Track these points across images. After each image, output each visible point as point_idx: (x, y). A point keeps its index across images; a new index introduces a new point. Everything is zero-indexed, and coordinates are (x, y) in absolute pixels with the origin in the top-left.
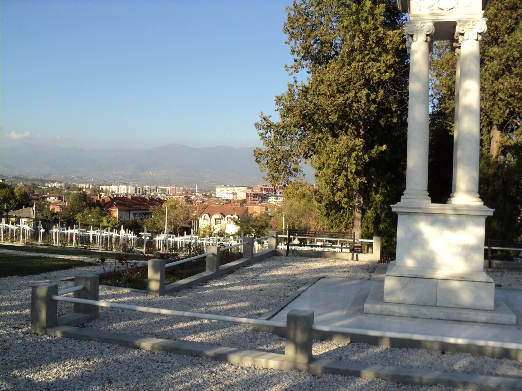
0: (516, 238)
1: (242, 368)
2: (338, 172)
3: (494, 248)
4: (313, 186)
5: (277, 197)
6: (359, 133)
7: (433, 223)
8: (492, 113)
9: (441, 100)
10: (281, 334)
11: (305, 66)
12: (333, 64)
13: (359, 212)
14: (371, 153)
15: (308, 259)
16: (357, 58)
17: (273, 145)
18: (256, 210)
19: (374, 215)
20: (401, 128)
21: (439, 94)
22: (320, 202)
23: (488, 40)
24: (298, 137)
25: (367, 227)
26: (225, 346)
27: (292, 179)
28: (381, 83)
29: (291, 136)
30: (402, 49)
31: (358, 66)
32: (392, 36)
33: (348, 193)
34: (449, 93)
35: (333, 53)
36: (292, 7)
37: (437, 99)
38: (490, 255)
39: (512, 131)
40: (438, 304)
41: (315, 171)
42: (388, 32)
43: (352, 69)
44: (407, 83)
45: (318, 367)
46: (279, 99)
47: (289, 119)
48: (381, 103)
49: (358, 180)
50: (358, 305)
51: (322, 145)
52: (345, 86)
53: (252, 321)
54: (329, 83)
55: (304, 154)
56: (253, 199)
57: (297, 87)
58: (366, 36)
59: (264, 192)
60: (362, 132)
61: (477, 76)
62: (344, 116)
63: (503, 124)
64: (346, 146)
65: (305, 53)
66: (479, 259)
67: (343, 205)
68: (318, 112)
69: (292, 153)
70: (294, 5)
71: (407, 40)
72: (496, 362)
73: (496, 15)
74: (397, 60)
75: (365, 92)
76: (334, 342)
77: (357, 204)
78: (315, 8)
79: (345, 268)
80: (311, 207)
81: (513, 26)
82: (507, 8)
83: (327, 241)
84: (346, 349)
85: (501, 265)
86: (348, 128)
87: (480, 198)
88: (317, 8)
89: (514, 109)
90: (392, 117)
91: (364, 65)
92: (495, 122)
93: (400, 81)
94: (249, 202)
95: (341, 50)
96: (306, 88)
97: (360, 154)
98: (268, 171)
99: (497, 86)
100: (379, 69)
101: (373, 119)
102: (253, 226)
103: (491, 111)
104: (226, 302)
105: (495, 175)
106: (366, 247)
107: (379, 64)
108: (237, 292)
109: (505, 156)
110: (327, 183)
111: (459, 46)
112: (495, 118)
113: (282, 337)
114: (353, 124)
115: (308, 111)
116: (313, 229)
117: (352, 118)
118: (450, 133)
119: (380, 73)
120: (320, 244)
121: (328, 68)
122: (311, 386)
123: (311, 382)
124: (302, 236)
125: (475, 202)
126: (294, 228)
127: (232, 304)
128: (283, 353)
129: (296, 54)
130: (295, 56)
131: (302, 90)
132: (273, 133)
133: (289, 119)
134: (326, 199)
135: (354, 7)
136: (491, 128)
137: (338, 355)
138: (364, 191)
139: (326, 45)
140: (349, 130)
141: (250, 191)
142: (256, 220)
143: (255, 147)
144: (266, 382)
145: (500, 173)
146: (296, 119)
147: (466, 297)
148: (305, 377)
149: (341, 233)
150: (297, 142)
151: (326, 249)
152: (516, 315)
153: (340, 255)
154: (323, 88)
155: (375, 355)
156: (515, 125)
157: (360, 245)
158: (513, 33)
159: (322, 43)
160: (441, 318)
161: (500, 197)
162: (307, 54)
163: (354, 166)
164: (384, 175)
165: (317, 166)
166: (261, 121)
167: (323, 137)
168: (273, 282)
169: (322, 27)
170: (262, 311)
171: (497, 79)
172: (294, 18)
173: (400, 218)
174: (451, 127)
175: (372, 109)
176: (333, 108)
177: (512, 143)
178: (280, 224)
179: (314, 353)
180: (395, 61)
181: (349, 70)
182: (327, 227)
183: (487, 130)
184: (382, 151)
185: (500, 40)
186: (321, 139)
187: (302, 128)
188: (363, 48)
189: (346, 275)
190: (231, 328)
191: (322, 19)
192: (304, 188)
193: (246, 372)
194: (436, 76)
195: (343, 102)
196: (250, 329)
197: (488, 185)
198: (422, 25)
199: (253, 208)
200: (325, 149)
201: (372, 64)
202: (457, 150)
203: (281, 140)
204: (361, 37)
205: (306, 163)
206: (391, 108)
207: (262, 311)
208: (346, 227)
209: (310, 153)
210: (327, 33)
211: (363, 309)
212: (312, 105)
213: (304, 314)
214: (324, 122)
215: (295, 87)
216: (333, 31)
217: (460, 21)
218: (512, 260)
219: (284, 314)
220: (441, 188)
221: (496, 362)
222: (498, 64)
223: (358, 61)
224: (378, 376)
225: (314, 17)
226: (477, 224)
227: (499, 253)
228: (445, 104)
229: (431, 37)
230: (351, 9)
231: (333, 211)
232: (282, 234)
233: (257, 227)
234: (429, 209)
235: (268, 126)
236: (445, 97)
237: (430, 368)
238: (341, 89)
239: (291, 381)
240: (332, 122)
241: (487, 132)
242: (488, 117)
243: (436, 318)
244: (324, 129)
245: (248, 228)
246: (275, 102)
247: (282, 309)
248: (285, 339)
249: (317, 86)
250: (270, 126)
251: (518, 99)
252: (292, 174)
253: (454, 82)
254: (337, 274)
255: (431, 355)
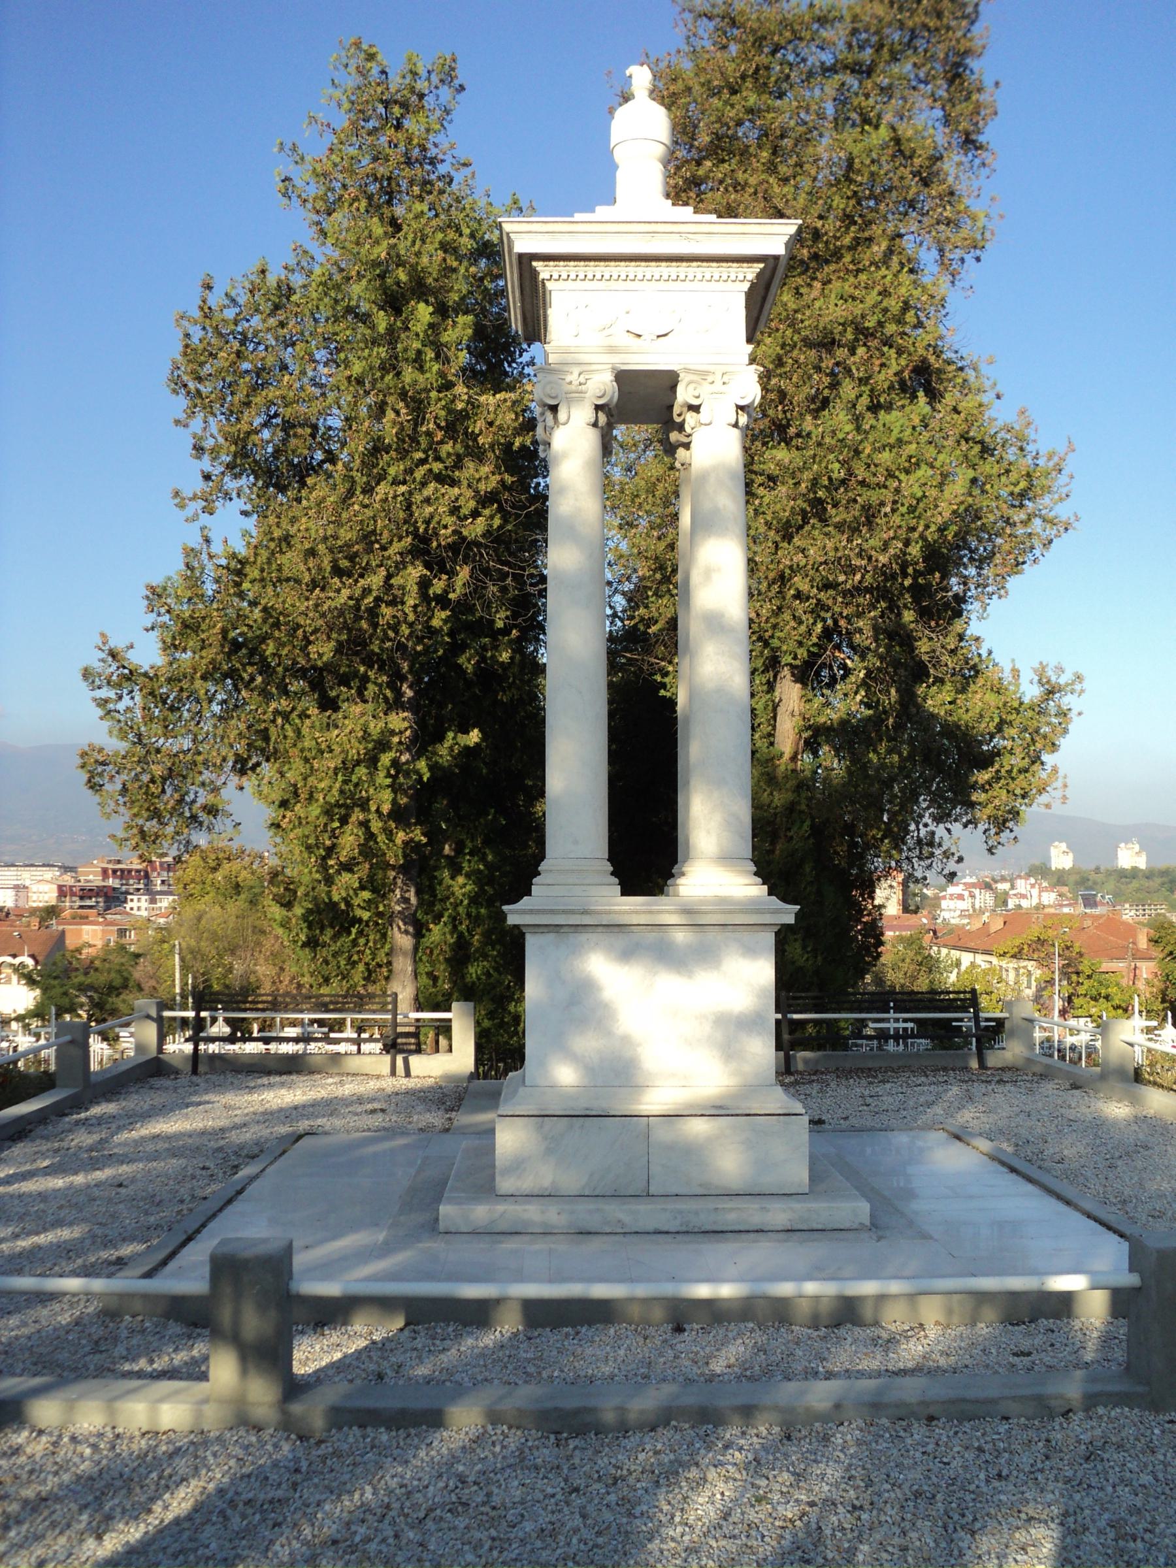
0: (854, 986)
1: (73, 1439)
2: (340, 812)
3: (796, 1016)
4: (262, 857)
5: (153, 896)
6: (399, 694)
7: (626, 955)
8: (778, 634)
9: (635, 599)
10: (191, 1317)
11: (234, 495)
12: (319, 489)
13: (406, 932)
14: (435, 753)
15: (260, 1081)
16: (392, 471)
17: (139, 736)
18: (91, 936)
19: (451, 940)
20: (521, 680)
21: (629, 579)
22: (288, 905)
23: (767, 427)
24: (216, 708)
25: (430, 974)
26: (14, 1375)
27: (201, 839)
28: (461, 547)
29: (196, 708)
30: (523, 447)
31: (395, 497)
32: (491, 409)
33: (371, 878)
34: (658, 576)
35: (319, 456)
36: (197, 314)
37: (624, 594)
38: (786, 1037)
39: (831, 685)
40: (652, 1190)
41: (270, 813)
42: (483, 399)
43: (377, 506)
44: (537, 547)
45: (313, 1411)
46: (156, 595)
47: (189, 653)
48: (462, 607)
49: (401, 836)
50: (420, 1209)
51: (290, 733)
52: (356, 554)
53: (98, 1285)
54: (307, 546)
55: (236, 762)
56: (78, 904)
57: (211, 557)
58: (418, 406)
59: (111, 882)
60: (409, 693)
61: (738, 528)
62: (354, 646)
63: (808, 664)
64: (360, 734)
65: (235, 456)
66: (762, 1050)
67: (359, 913)
68: (277, 634)
69: (200, 759)
70: (201, 308)
71: (540, 419)
72: (824, 1338)
73: (779, 362)
74: (509, 479)
75: (415, 572)
76: (357, 1328)
77: (398, 908)
78: (264, 321)
79: (372, 1100)
80: (258, 923)
81: (826, 392)
82: (808, 343)
83: (312, 1022)
84: (393, 1345)
85: (817, 1061)
86: (365, 679)
87: (756, 874)
88: (272, 322)
89: (836, 622)
90: (495, 648)
91: (410, 493)
92: (788, 659)
93: (516, 541)
94: (67, 914)
95: (342, 447)
96: (240, 562)
97: (403, 759)
98: (126, 814)
99: (788, 556)
100: (455, 506)
101: (441, 652)
102: (82, 988)
103: (775, 627)
104: (10, 1230)
105: (791, 808)
106: (431, 1035)
107: (456, 491)
108: (42, 1196)
109: (815, 754)
110: (309, 848)
111: (686, 440)
112: (784, 648)
113: (196, 1325)
114: (380, 669)
115: (245, 629)
116: (267, 988)
117: (377, 650)
118: (662, 693)
119: (459, 518)
120: (291, 1032)
121: (304, 502)
122: (297, 1471)
123: (297, 1460)
124: (234, 1010)
125: (745, 887)
126: (211, 986)
127: (29, 1234)
128: (204, 1377)
129: (206, 458)
130: (206, 464)
131: (227, 568)
132: (138, 698)
133: (189, 653)
134: (307, 895)
135: (382, 321)
136: (775, 677)
137: (372, 1367)
138: (420, 867)
139: (299, 431)
140: (370, 686)
141: (68, 879)
142: (90, 967)
143: (83, 742)
144: (154, 1475)
145: (804, 801)
146: (210, 653)
147: (730, 1164)
148: (275, 1446)
149: (353, 996)
150: (215, 726)
151: (313, 1047)
152: (869, 1200)
153: (354, 1064)
154: (291, 561)
155: (482, 1355)
156: (839, 668)
157: (412, 1029)
158: (826, 412)
159: (288, 426)
160: (665, 1229)
161: (808, 870)
162: (242, 458)
163: (387, 795)
164: (478, 816)
165: (277, 796)
166: (103, 660)
167: (294, 709)
168: (155, 1156)
169: (286, 378)
170: (127, 1250)
171: (788, 538)
172: (201, 347)
173: (532, 943)
174: (666, 674)
175: (436, 623)
176: (320, 622)
177: (834, 716)
178: (165, 977)
179: (299, 1369)
180: (502, 481)
181: (366, 506)
182: (311, 980)
183: (764, 680)
184: (467, 748)
185: (792, 431)
186: (286, 716)
187: (229, 681)
188: (408, 441)
189: (377, 1121)
190: (32, 1314)
191: (287, 354)
192: (236, 865)
193: (88, 1451)
194: (621, 527)
195: (351, 603)
196: (91, 1310)
197: (774, 837)
198: (582, 379)
199: (79, 933)
200: (300, 745)
201: (436, 490)
202: (687, 739)
203: (165, 720)
204: (404, 411)
205: (242, 788)
206: (493, 621)
207: (127, 1250)
208: (369, 978)
209: (254, 760)
210: (303, 394)
211: (437, 1220)
212: (257, 613)
213: (261, 1250)
214: (295, 663)
215: (204, 556)
216: (317, 392)
217: (687, 370)
218: (846, 1048)
219: (198, 1254)
220: (645, 851)
221: (824, 1338)
222: (789, 497)
223: (396, 482)
224: (494, 1417)
225: (262, 347)
226: (750, 951)
227: (810, 1029)
228: (647, 607)
229: (609, 415)
230: (373, 327)
231: (329, 932)
232: (172, 1009)
233: (96, 991)
234: (616, 912)
235: (124, 676)
236: (647, 588)
237: (643, 1377)
238: (344, 564)
239: (232, 1462)
240: (319, 663)
241: (765, 688)
242: (766, 644)
243: (651, 1228)
244: (296, 686)
245: (65, 994)
246: (146, 602)
247: (189, 1239)
248: (207, 1332)
249: (273, 554)
250: (130, 676)
251: (845, 594)
252: (201, 824)
253: (672, 547)
254: (353, 1122)
255: (646, 1338)
